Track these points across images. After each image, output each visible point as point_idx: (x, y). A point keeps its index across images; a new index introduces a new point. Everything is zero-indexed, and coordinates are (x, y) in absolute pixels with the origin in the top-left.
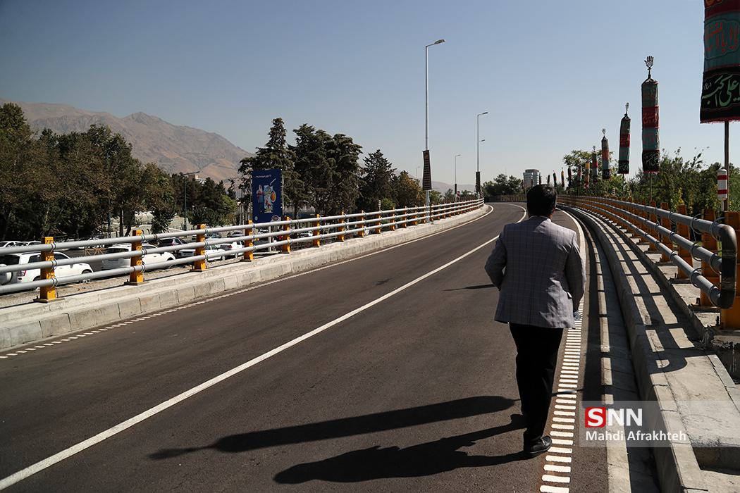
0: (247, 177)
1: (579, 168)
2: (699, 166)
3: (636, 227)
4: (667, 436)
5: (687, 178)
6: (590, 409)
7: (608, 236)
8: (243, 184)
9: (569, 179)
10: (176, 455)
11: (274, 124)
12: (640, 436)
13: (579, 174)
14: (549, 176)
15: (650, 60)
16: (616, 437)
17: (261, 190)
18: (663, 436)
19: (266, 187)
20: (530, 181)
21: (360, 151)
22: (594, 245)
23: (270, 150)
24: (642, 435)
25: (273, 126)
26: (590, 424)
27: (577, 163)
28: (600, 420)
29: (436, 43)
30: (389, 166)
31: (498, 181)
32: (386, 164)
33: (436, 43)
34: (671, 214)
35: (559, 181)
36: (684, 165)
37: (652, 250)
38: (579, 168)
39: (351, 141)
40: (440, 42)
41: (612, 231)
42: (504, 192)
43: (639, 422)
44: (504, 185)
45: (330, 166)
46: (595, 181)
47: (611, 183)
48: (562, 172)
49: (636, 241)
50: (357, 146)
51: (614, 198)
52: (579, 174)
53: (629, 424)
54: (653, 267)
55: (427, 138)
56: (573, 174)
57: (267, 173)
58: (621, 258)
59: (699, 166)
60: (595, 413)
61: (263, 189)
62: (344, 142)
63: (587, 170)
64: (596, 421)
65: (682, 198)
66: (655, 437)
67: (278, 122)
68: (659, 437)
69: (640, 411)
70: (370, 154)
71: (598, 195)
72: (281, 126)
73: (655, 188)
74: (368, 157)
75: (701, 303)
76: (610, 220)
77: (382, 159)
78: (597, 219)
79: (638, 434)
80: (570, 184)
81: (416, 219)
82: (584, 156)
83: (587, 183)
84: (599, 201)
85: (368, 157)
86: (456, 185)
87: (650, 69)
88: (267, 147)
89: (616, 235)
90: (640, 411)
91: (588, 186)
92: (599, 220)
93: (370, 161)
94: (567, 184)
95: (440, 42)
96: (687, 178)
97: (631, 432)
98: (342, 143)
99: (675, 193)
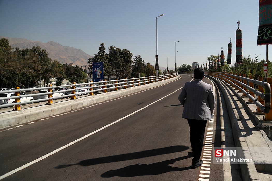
0: (91, 65)
1: (213, 62)
2: (257, 61)
3: (234, 83)
4: (245, 160)
5: (253, 65)
6: (217, 150)
7: (224, 87)
8: (89, 68)
9: (209, 66)
10: (65, 167)
11: (101, 45)
12: (235, 160)
13: (213, 64)
14: (202, 65)
15: (239, 22)
16: (227, 160)
17: (96, 70)
18: (244, 160)
19: (98, 68)
20: (195, 66)
21: (132, 55)
22: (218, 90)
23: (99, 55)
24: (236, 160)
25: (100, 46)
26: (217, 155)
27: (212, 60)
28: (221, 154)
29: (160, 16)
30: (143, 61)
31: (183, 66)
32: (142, 60)
33: (160, 16)
34: (247, 79)
35: (205, 66)
36: (251, 61)
37: (240, 92)
38: (213, 62)
39: (129, 52)
40: (162, 15)
41: (225, 85)
42: (185, 70)
43: (235, 155)
44: (185, 68)
45: (121, 61)
46: (219, 66)
47: (225, 67)
48: (207, 63)
49: (234, 88)
50: (131, 54)
51: (226, 73)
52: (213, 64)
53: (231, 156)
54: (240, 98)
55: (157, 51)
56: (210, 64)
57: (98, 63)
58: (228, 95)
59: (257, 61)
60: (219, 152)
61: (97, 69)
62: (126, 52)
63: (216, 63)
64: (219, 155)
65: (251, 73)
66: (241, 160)
67: (102, 45)
68: (242, 160)
69: (235, 151)
70: (136, 57)
71: (220, 72)
72: (103, 46)
73: (241, 69)
74: (135, 58)
75: (258, 111)
76: (224, 81)
77: (140, 58)
78: (219, 80)
79: (234, 159)
80: (209, 68)
81: (153, 80)
82: (215, 57)
83: (216, 67)
84: (220, 74)
85: (135, 58)
86: (168, 68)
87: (239, 25)
88: (98, 54)
89: (226, 86)
90: (235, 151)
91: (216, 68)
92: (220, 81)
93: (136, 59)
94: (208, 67)
95: (162, 15)
96: (253, 65)
97: (232, 159)
98: (126, 53)
99: (248, 71)
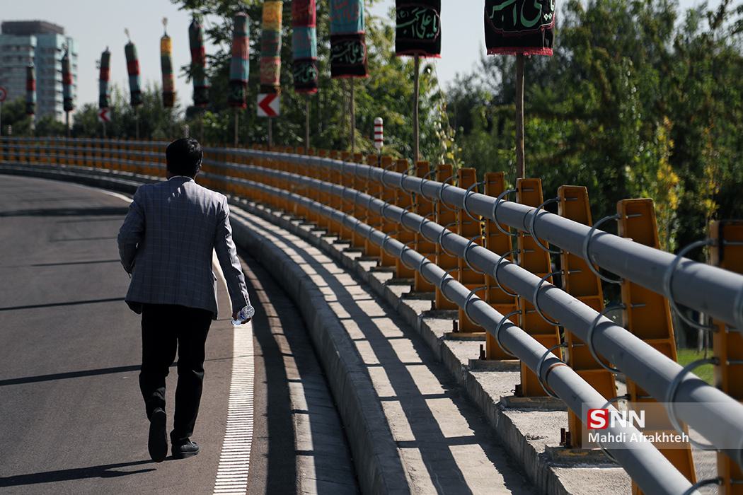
1: (239, 22)
4: (670, 438)
5: (695, 75)
7: (353, 330)
9: (195, 70)
10: (123, 475)
13: (237, 50)
14: (106, 57)
18: (666, 438)
20: (20, 75)
22: (292, 370)
26: (593, 425)
28: (603, 422)
34: (592, 240)
35: (150, 78)
36: (680, 22)
37: (530, 393)
38: (239, 22)
41: (371, 307)
46: (305, 85)
47: (378, 95)
48: (165, 40)
49: (466, 351)
51: (382, 161)
52: (237, 50)
54: (534, 469)
56: (210, 48)
58: (402, 429)
63: (270, 35)
64: (598, 415)
65: (671, 161)
68: (661, 438)
69: (643, 413)
71: (320, 145)
73: (560, 117)
76: (365, 258)
78: (313, 251)
80: (198, 92)
83: (270, 91)
84: (323, 172)
89: (388, 327)
90: (643, 413)
91: (276, 105)
92: (321, 258)
94: (184, 93)
96: (695, 75)
99: (644, 139)
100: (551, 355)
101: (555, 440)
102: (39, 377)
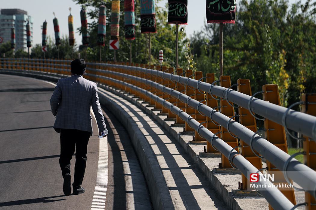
1: (102, 9)
4: (285, 186)
5: (296, 32)
7: (150, 140)
9: (83, 30)
10: (52, 201)
13: (101, 21)
14: (45, 24)
18: (283, 186)
20: (9, 32)
22: (124, 157)
26: (252, 180)
28: (256, 179)
34: (252, 102)
35: (64, 33)
36: (289, 9)
37: (225, 167)
38: (102, 9)
41: (158, 130)
46: (130, 36)
47: (161, 40)
48: (70, 17)
49: (198, 149)
51: (163, 68)
52: (101, 21)
54: (227, 199)
56: (89, 20)
58: (171, 182)
63: (115, 15)
64: (254, 176)
65: (286, 68)
68: (281, 186)
69: (273, 175)
71: (136, 62)
73: (238, 50)
76: (155, 109)
78: (133, 107)
80: (84, 39)
83: (115, 38)
84: (137, 73)
89: (165, 139)
90: (273, 175)
91: (117, 45)
92: (136, 109)
94: (78, 39)
96: (296, 32)
99: (274, 59)
100: (234, 151)
101: (236, 187)
102: (17, 160)
